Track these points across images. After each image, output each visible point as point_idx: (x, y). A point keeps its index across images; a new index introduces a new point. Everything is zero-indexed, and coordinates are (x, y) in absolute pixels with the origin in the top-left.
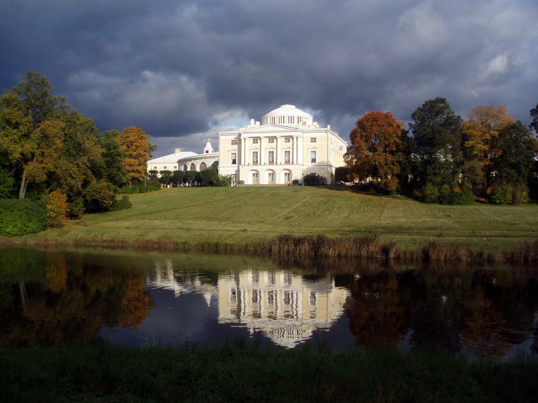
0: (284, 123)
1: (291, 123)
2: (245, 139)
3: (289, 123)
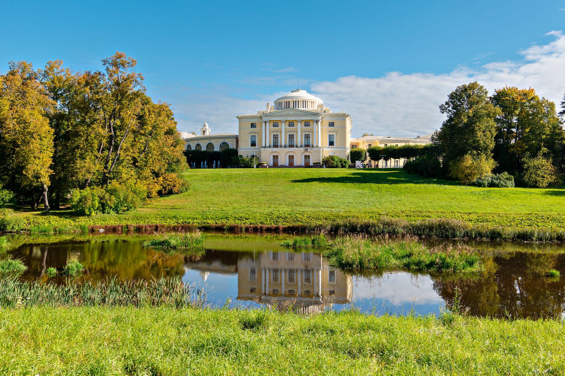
0: (298, 107)
1: (305, 107)
2: (266, 122)
3: (303, 107)
